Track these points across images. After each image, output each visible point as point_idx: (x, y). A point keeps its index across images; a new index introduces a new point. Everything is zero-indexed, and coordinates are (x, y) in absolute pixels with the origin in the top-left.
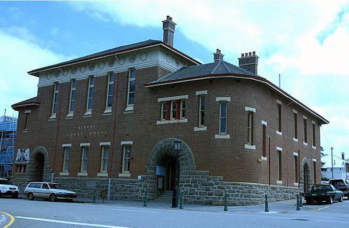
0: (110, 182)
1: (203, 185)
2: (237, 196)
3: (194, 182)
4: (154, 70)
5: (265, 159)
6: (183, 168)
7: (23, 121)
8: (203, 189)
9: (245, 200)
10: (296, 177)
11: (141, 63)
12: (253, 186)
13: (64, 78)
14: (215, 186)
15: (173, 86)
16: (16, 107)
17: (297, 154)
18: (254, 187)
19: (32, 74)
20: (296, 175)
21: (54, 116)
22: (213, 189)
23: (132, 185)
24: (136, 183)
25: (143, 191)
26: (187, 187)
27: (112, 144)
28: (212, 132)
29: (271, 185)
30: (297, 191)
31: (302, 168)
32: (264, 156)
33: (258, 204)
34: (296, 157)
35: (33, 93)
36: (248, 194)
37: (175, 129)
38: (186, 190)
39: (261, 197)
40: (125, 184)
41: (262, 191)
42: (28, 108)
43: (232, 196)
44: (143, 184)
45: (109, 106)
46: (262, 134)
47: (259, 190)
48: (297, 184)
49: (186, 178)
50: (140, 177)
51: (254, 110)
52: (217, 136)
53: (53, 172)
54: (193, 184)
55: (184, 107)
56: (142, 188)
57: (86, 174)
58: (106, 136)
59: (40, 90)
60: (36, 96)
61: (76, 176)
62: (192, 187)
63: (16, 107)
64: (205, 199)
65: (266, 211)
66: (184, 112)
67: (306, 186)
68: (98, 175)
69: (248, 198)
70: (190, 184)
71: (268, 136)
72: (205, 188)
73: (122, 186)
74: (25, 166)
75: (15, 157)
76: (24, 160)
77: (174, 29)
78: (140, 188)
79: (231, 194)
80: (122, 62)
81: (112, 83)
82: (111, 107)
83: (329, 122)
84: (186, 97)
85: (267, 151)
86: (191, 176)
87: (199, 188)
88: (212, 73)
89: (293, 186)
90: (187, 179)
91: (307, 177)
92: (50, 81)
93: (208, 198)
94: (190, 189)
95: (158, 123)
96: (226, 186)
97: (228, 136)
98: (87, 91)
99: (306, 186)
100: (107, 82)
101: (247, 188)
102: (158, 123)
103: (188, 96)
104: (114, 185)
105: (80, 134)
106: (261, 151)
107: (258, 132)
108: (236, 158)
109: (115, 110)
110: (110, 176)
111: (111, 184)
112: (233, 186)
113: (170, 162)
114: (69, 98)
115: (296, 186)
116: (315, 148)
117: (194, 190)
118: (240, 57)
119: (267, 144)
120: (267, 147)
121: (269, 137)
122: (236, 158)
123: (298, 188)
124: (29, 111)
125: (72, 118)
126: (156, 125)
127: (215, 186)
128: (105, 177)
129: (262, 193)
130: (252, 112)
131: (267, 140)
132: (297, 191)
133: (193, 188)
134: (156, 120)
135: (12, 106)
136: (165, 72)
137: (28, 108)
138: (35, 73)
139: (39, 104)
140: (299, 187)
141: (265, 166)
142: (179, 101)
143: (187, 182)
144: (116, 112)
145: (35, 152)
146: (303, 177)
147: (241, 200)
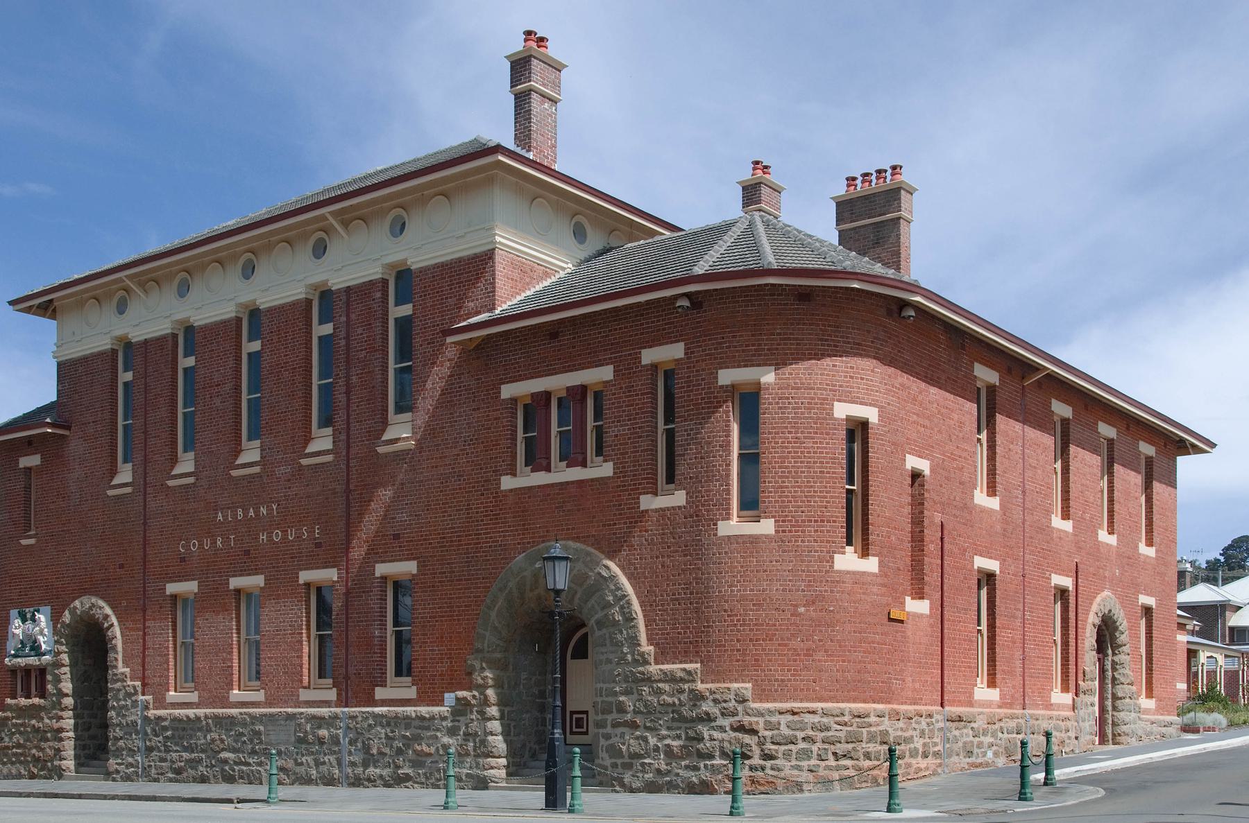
2: (806, 754)
5: (919, 607)
6: (603, 657)
9: (838, 768)
10: (1065, 674)
12: (868, 716)
13: (151, 319)
14: (721, 721)
15: (553, 331)
17: (1067, 582)
18: (873, 719)
19: (28, 310)
20: (1065, 659)
21: (125, 475)
22: (716, 734)
29: (947, 708)
31: (1089, 638)
32: (919, 595)
34: (1062, 593)
35: (46, 393)
36: (850, 746)
41: (907, 734)
43: (787, 755)
46: (908, 509)
48: (1067, 698)
51: (871, 414)
55: (598, 415)
58: (318, 545)
59: (67, 372)
65: (889, 810)
67: (1109, 703)
68: (377, 697)
69: (848, 763)
71: (934, 517)
76: (36, 649)
77: (557, 85)
79: (783, 748)
81: (328, 329)
82: (329, 431)
83: (1213, 445)
84: (605, 373)
85: (932, 578)
88: (699, 270)
89: (1049, 706)
91: (1114, 669)
92: (98, 333)
95: (507, 483)
96: (761, 720)
98: (238, 370)
99: (1109, 703)
101: (846, 724)
102: (507, 483)
103: (611, 367)
105: (226, 540)
106: (905, 579)
107: (889, 505)
108: (802, 610)
109: (344, 444)
112: (790, 717)
113: (557, 636)
114: (238, 388)
115: (1060, 707)
116: (1151, 552)
117: (645, 740)
118: (841, 190)
119: (932, 547)
121: (938, 520)
122: (802, 610)
123: (1069, 714)
124: (33, 461)
125: (257, 469)
126: (501, 496)
127: (721, 721)
130: (864, 424)
131: (931, 535)
134: (498, 473)
136: (526, 271)
138: (43, 305)
139: (69, 428)
141: (920, 638)
142: (579, 392)
144: (348, 447)
147: (822, 772)
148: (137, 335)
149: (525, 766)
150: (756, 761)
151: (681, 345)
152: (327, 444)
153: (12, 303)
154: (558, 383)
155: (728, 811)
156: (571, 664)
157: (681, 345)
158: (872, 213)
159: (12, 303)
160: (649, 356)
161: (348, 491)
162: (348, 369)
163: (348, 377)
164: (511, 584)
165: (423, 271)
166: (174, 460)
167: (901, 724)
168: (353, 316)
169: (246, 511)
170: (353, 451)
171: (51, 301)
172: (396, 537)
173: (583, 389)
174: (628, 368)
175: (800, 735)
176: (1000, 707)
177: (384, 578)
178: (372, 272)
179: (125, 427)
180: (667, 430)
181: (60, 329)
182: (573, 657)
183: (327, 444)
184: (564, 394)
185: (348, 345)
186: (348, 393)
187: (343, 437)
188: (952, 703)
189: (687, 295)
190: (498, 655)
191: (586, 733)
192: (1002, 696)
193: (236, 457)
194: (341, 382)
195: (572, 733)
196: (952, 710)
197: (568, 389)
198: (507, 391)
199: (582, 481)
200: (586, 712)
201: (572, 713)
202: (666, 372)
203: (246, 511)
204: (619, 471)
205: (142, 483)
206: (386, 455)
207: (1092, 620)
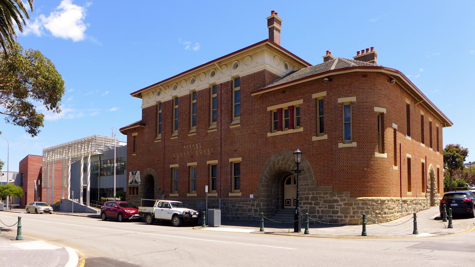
0: (220, 202)
1: (325, 201)
3: (314, 198)
4: (262, 77)
5: (396, 168)
7: (132, 143)
8: (326, 207)
11: (246, 69)
13: (167, 96)
14: (340, 203)
16: (124, 131)
19: (135, 96)
23: (245, 204)
24: (248, 203)
25: (256, 211)
26: (306, 205)
27: (221, 161)
28: (333, 141)
30: (424, 201)
31: (429, 176)
32: (396, 165)
33: (391, 220)
35: (138, 117)
37: (289, 140)
38: (305, 208)
39: (393, 213)
40: (236, 203)
42: (135, 130)
44: (256, 203)
45: (214, 121)
47: (392, 205)
49: (304, 194)
50: (252, 196)
52: (341, 145)
53: (163, 194)
54: (313, 202)
56: (255, 208)
57: (196, 195)
58: (213, 154)
59: (145, 111)
60: (141, 119)
61: (228, 196)
62: (312, 204)
63: (124, 131)
64: (330, 218)
66: (298, 119)
70: (310, 201)
72: (329, 206)
73: (233, 206)
74: (137, 188)
75: (128, 179)
76: (136, 182)
78: (253, 208)
80: (223, 71)
81: (215, 95)
82: (216, 123)
83: (453, 124)
84: (301, 102)
86: (311, 192)
87: (321, 206)
88: (333, 68)
90: (306, 195)
92: (152, 101)
93: (332, 216)
94: (310, 207)
97: (354, 144)
98: (190, 108)
100: (210, 95)
104: (225, 204)
108: (365, 169)
110: (220, 196)
111: (221, 204)
117: (315, 207)
120: (398, 154)
123: (425, 198)
126: (267, 138)
128: (215, 197)
129: (394, 208)
130: (382, 114)
131: (398, 146)
132: (424, 201)
133: (313, 206)
134: (266, 132)
135: (121, 129)
137: (135, 130)
138: (138, 94)
139: (145, 125)
140: (426, 197)
143: (305, 200)
145: (145, 174)
146: (429, 186)
148: (163, 101)
149: (274, 215)
150: (352, 214)
151: (325, 92)
152: (195, 130)
153: (131, 94)
154: (285, 106)
155: (361, 234)
156: (286, 186)
157: (325, 92)
158: (369, 56)
159: (131, 94)
160: (314, 96)
161: (221, 139)
162: (221, 106)
163: (221, 108)
164: (270, 163)
165: (243, 77)
166: (172, 132)
167: (393, 203)
168: (223, 91)
169: (192, 145)
170: (222, 128)
171: (141, 93)
172: (235, 151)
173: (293, 107)
174: (307, 100)
175: (365, 207)
176: (412, 197)
177: (232, 162)
178: (228, 79)
179: (159, 125)
180: (320, 118)
181: (143, 101)
182: (287, 184)
183: (195, 130)
184: (276, 111)
185: (221, 99)
186: (221, 112)
187: (220, 124)
188: (404, 196)
189: (326, 77)
190: (266, 183)
191: (290, 205)
192: (412, 193)
193: (189, 131)
194: (219, 109)
195: (286, 205)
196: (404, 198)
197: (288, 107)
198: (269, 109)
199: (293, 133)
200: (290, 200)
201: (286, 200)
202: (274, 113)
203: (192, 145)
204: (306, 130)
205: (164, 139)
206: (232, 128)
207: (429, 171)
